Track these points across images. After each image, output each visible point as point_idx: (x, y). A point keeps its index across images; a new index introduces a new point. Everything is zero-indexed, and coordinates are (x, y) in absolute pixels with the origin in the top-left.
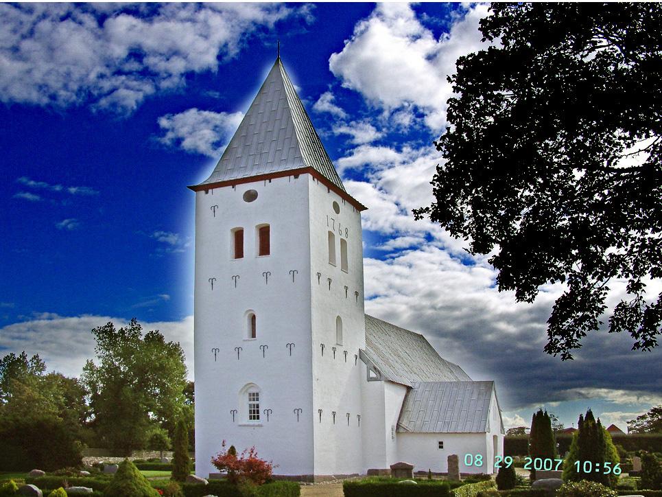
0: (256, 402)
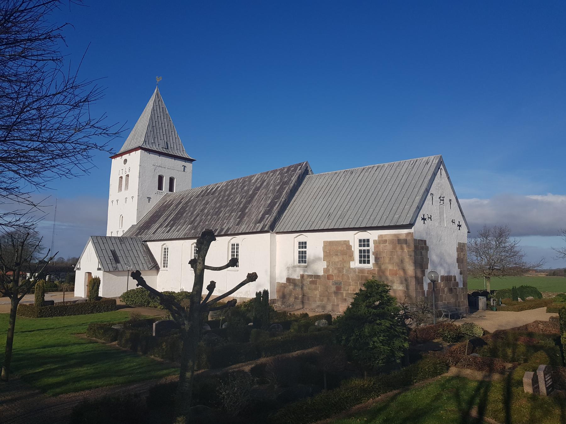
0: (366, 248)
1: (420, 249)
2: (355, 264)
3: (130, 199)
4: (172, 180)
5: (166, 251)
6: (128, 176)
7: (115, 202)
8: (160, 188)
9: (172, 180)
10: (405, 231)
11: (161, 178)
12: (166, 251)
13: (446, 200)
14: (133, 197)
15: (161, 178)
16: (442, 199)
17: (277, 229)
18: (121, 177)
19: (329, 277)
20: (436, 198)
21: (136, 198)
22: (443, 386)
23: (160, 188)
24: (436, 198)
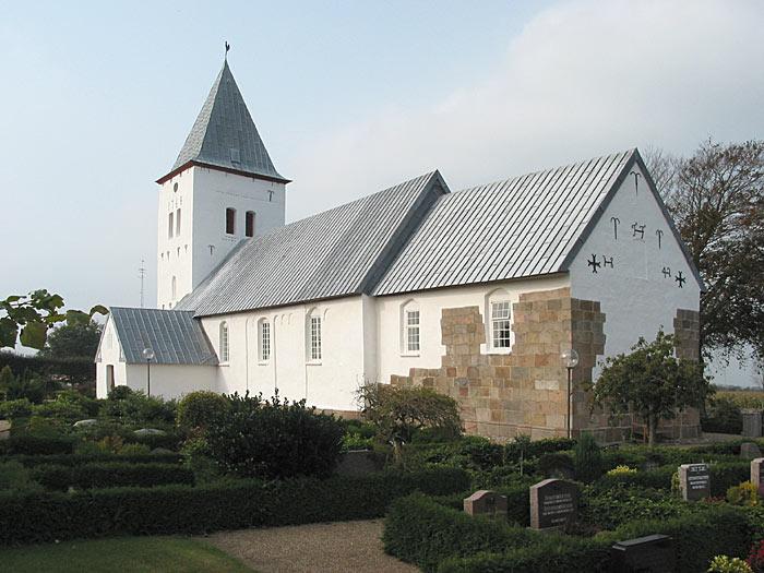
1: (587, 317)
2: (488, 348)
3: (182, 250)
4: (250, 217)
5: (224, 331)
6: (179, 211)
7: (165, 255)
8: (230, 229)
9: (250, 217)
10: (550, 287)
11: (230, 213)
12: (224, 331)
13: (650, 232)
14: (186, 246)
15: (230, 213)
16: (640, 231)
17: (380, 290)
18: (171, 214)
19: (451, 371)
20: (625, 227)
21: (190, 248)
22: (32, 454)
23: (230, 229)
24: (625, 227)
